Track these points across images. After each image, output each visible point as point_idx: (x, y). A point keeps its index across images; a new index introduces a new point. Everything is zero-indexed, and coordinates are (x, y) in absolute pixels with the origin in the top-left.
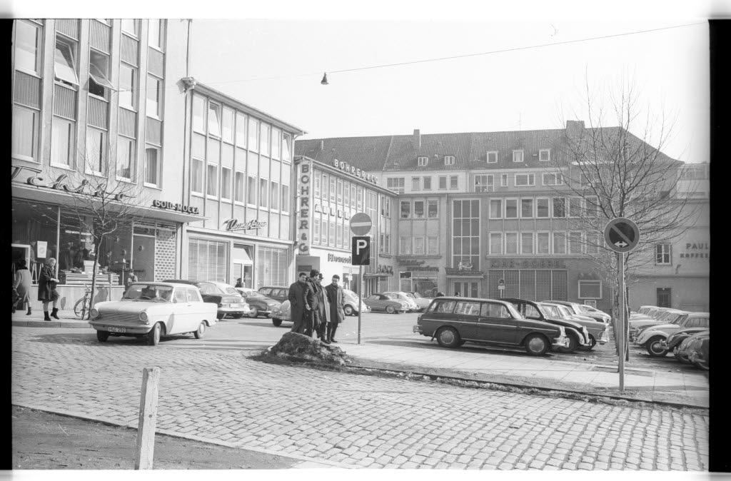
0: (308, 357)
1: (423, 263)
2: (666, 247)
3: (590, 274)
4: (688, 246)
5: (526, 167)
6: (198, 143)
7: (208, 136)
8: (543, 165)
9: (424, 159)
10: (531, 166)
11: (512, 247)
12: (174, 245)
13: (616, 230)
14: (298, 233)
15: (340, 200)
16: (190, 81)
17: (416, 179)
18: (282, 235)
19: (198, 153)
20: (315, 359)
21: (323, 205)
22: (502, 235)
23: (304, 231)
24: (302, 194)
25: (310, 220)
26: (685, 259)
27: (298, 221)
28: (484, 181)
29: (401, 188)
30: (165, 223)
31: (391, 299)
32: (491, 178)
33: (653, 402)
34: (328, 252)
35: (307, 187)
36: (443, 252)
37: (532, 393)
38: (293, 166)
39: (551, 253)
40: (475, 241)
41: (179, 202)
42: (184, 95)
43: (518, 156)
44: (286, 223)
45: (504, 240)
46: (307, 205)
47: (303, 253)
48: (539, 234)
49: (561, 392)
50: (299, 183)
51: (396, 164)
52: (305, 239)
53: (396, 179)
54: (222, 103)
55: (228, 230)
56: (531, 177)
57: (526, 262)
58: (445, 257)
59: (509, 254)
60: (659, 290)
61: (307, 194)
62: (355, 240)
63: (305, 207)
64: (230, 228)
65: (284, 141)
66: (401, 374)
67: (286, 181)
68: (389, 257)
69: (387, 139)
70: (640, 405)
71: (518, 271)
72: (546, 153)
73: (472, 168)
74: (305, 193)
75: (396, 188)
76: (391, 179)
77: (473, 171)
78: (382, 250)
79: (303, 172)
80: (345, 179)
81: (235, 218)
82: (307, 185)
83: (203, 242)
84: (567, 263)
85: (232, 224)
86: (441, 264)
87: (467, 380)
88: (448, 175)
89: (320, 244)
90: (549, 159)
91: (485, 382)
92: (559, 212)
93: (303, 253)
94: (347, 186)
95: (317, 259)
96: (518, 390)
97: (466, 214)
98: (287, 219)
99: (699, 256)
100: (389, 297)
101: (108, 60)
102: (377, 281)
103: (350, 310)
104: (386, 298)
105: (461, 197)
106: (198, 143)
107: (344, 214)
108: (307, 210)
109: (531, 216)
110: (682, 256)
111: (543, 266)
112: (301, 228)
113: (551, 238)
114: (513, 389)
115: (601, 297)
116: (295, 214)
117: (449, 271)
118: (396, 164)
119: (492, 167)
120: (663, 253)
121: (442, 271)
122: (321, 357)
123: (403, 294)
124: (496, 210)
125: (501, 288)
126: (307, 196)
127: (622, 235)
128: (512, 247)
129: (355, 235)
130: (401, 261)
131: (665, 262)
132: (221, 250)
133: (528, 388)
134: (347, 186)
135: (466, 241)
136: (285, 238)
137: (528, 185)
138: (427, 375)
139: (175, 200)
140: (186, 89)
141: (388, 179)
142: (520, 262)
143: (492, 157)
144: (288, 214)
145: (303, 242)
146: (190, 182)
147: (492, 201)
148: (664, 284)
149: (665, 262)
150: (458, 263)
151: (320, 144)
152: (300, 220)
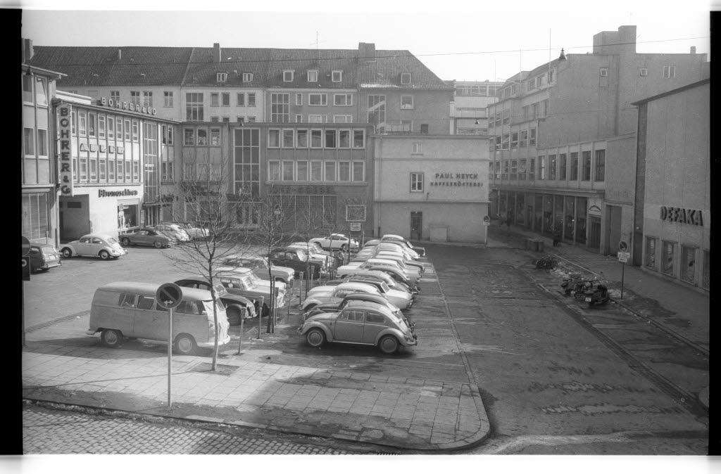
2: (420, 176)
8: (336, 86)
9: (223, 75)
11: (289, 177)
14: (60, 175)
17: (215, 95)
23: (66, 173)
26: (434, 187)
27: (59, 162)
32: (286, 96)
34: (97, 189)
35: (67, 131)
37: (101, 414)
38: (50, 109)
39: (324, 180)
40: (256, 168)
43: (313, 76)
45: (282, 170)
46: (68, 148)
47: (65, 195)
51: (196, 79)
53: (195, 94)
57: (300, 189)
59: (287, 181)
60: (413, 213)
61: (67, 137)
68: (172, 184)
69: (187, 51)
73: (268, 87)
74: (65, 136)
75: (195, 103)
76: (190, 94)
77: (270, 89)
78: (164, 177)
79: (62, 115)
80: (116, 115)
82: (67, 128)
86: (224, 190)
88: (246, 92)
89: (88, 181)
90: (341, 80)
91: (71, 405)
92: (331, 142)
93: (65, 195)
97: (247, 143)
98: (47, 164)
99: (449, 184)
100: (158, 232)
102: (159, 209)
103: (106, 254)
104: (155, 234)
108: (68, 153)
110: (432, 184)
111: (316, 192)
112: (62, 170)
115: (365, 220)
116: (56, 157)
117: (230, 197)
118: (196, 79)
120: (417, 182)
124: (274, 139)
126: (68, 139)
127: (168, 295)
128: (289, 177)
130: (184, 186)
131: (419, 189)
137: (321, 105)
138: (29, 399)
141: (187, 94)
145: (65, 184)
147: (271, 131)
148: (417, 209)
149: (419, 189)
151: (117, 53)
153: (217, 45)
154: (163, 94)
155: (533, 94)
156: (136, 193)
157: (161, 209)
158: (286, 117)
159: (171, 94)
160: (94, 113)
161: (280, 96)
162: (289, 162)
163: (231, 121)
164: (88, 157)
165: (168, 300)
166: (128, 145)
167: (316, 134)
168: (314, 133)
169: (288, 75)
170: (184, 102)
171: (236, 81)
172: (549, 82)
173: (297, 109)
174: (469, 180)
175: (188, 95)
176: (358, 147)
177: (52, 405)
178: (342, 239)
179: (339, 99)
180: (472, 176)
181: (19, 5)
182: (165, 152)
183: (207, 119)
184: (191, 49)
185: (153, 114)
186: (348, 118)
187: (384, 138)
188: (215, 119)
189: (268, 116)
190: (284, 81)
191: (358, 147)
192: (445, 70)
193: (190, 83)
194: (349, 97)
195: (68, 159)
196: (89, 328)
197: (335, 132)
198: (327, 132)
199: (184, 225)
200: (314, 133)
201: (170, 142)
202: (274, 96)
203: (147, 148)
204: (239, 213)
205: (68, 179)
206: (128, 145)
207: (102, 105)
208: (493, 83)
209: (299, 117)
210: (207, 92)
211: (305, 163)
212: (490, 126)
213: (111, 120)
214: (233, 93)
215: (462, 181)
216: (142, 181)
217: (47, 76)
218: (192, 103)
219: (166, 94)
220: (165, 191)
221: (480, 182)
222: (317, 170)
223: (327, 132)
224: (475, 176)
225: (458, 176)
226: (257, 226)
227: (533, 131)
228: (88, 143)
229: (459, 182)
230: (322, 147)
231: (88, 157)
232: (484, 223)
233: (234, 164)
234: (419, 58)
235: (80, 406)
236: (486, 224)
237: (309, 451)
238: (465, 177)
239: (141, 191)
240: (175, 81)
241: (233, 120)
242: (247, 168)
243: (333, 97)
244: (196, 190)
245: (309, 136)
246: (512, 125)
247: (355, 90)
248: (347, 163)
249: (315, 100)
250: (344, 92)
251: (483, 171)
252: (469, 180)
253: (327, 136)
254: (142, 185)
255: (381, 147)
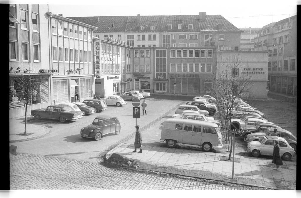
0: (124, 165)
1: (144, 75)
3: (208, 80)
4: (245, 69)
5: (183, 32)
6: (54, 39)
7: (58, 36)
8: (191, 31)
10: (186, 31)
12: (48, 85)
13: (234, 126)
15: (111, 54)
16: (50, 14)
17: (139, 36)
18: (89, 73)
19: (54, 44)
20: (126, 166)
21: (105, 57)
22: (175, 64)
23: (98, 70)
24: (97, 54)
25: (100, 65)
28: (167, 37)
29: (133, 39)
30: (43, 77)
31: (134, 95)
33: (243, 185)
35: (99, 52)
36: (152, 70)
37: (204, 181)
38: (92, 42)
39: (194, 71)
40: (165, 66)
41: (49, 69)
42: (47, 20)
43: (180, 27)
44: (91, 67)
46: (99, 59)
47: (97, 79)
48: (189, 64)
49: (214, 181)
50: (95, 49)
52: (99, 73)
53: (130, 36)
54: (63, 20)
55: (68, 74)
56: (185, 36)
57: (184, 75)
58: (153, 73)
61: (99, 54)
62: (134, 108)
63: (98, 60)
64: (69, 73)
65: (88, 31)
66: (159, 173)
67: (90, 50)
68: (130, 73)
69: (126, 17)
70: (239, 186)
71: (181, 79)
72: (191, 26)
73: (162, 32)
74: (98, 54)
75: (131, 39)
76: (131, 36)
77: (162, 33)
80: (112, 45)
81: (71, 69)
82: (99, 50)
83: (59, 81)
84: (200, 75)
85: (70, 72)
86: (151, 76)
87: (182, 176)
88: (152, 34)
89: (104, 73)
90: (192, 28)
91: (188, 176)
92: (197, 55)
93: (97, 79)
94: (114, 47)
95: (103, 79)
96: (200, 180)
97: (161, 56)
100: (133, 94)
101: (15, 9)
103: (119, 104)
105: (159, 49)
106: (54, 39)
107: (113, 59)
108: (99, 61)
109: (186, 57)
110: (242, 73)
111: (184, 77)
112: (97, 68)
113: (182, 66)
114: (198, 179)
117: (154, 79)
119: (169, 31)
121: (152, 78)
122: (128, 165)
123: (138, 92)
124: (172, 54)
125: (175, 86)
127: (235, 127)
129: (134, 107)
130: (135, 74)
132: (66, 82)
133: (203, 179)
134: (114, 47)
135: (161, 66)
136: (91, 74)
139: (47, 68)
140: (48, 17)
141: (127, 36)
142: (182, 75)
143: (170, 27)
144: (91, 63)
145: (98, 74)
146: (52, 57)
147: (171, 50)
150: (158, 76)
151: (97, 19)
152: (96, 66)
153: (139, 15)
154: (104, 36)
155: (278, 33)
156: (119, 78)
157: (127, 84)
158: (169, 45)
159: (121, 36)
160: (106, 44)
161: (167, 36)
162: (179, 64)
163: (146, 47)
164: (104, 63)
165: (235, 129)
166: (116, 57)
167: (179, 52)
168: (178, 51)
169: (170, 27)
170: (126, 39)
171: (147, 30)
172: (288, 27)
173: (174, 41)
174: (259, 71)
175: (128, 36)
176: (209, 57)
177: (179, 176)
178: (209, 97)
179: (192, 36)
180: (260, 69)
181: (8, 2)
182: (128, 60)
183: (136, 46)
184: (127, 17)
185: (125, 44)
186: (195, 45)
187: (222, 53)
188: (139, 46)
189: (161, 45)
190: (189, 29)
191: (209, 57)
192: (239, 24)
193: (128, 31)
194: (196, 36)
195: (99, 64)
196: (160, 138)
197: (199, 50)
198: (196, 51)
199: (141, 92)
200: (178, 51)
201: (129, 56)
202: (164, 36)
203: (123, 59)
204: (158, 85)
205: (99, 72)
206: (116, 57)
207: (109, 40)
208: (253, 28)
209: (175, 45)
210: (136, 35)
211: (186, 64)
212: (255, 47)
213: (111, 47)
214: (147, 35)
215: (256, 71)
216: (121, 73)
217: (91, 29)
218: (129, 39)
219: (119, 36)
220: (128, 77)
221: (25, 69)
222: (179, 67)
223: (196, 51)
224: (262, 69)
225: (254, 69)
226: (165, 92)
227: (281, 50)
228: (104, 56)
229: (255, 72)
230: (193, 57)
231: (104, 63)
232: (266, 90)
233: (156, 65)
234: (226, 19)
235: (193, 177)
236: (267, 90)
237: (125, 188)
238: (257, 69)
239: (120, 76)
240: (123, 30)
241: (147, 46)
242: (161, 66)
243: (189, 36)
244: (138, 76)
245: (176, 53)
246: (268, 47)
247: (198, 33)
248: (205, 64)
249: (181, 37)
250: (194, 34)
251: (265, 66)
252: (259, 71)
253: (195, 52)
254: (121, 74)
255: (219, 56)
